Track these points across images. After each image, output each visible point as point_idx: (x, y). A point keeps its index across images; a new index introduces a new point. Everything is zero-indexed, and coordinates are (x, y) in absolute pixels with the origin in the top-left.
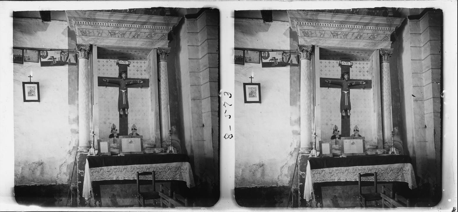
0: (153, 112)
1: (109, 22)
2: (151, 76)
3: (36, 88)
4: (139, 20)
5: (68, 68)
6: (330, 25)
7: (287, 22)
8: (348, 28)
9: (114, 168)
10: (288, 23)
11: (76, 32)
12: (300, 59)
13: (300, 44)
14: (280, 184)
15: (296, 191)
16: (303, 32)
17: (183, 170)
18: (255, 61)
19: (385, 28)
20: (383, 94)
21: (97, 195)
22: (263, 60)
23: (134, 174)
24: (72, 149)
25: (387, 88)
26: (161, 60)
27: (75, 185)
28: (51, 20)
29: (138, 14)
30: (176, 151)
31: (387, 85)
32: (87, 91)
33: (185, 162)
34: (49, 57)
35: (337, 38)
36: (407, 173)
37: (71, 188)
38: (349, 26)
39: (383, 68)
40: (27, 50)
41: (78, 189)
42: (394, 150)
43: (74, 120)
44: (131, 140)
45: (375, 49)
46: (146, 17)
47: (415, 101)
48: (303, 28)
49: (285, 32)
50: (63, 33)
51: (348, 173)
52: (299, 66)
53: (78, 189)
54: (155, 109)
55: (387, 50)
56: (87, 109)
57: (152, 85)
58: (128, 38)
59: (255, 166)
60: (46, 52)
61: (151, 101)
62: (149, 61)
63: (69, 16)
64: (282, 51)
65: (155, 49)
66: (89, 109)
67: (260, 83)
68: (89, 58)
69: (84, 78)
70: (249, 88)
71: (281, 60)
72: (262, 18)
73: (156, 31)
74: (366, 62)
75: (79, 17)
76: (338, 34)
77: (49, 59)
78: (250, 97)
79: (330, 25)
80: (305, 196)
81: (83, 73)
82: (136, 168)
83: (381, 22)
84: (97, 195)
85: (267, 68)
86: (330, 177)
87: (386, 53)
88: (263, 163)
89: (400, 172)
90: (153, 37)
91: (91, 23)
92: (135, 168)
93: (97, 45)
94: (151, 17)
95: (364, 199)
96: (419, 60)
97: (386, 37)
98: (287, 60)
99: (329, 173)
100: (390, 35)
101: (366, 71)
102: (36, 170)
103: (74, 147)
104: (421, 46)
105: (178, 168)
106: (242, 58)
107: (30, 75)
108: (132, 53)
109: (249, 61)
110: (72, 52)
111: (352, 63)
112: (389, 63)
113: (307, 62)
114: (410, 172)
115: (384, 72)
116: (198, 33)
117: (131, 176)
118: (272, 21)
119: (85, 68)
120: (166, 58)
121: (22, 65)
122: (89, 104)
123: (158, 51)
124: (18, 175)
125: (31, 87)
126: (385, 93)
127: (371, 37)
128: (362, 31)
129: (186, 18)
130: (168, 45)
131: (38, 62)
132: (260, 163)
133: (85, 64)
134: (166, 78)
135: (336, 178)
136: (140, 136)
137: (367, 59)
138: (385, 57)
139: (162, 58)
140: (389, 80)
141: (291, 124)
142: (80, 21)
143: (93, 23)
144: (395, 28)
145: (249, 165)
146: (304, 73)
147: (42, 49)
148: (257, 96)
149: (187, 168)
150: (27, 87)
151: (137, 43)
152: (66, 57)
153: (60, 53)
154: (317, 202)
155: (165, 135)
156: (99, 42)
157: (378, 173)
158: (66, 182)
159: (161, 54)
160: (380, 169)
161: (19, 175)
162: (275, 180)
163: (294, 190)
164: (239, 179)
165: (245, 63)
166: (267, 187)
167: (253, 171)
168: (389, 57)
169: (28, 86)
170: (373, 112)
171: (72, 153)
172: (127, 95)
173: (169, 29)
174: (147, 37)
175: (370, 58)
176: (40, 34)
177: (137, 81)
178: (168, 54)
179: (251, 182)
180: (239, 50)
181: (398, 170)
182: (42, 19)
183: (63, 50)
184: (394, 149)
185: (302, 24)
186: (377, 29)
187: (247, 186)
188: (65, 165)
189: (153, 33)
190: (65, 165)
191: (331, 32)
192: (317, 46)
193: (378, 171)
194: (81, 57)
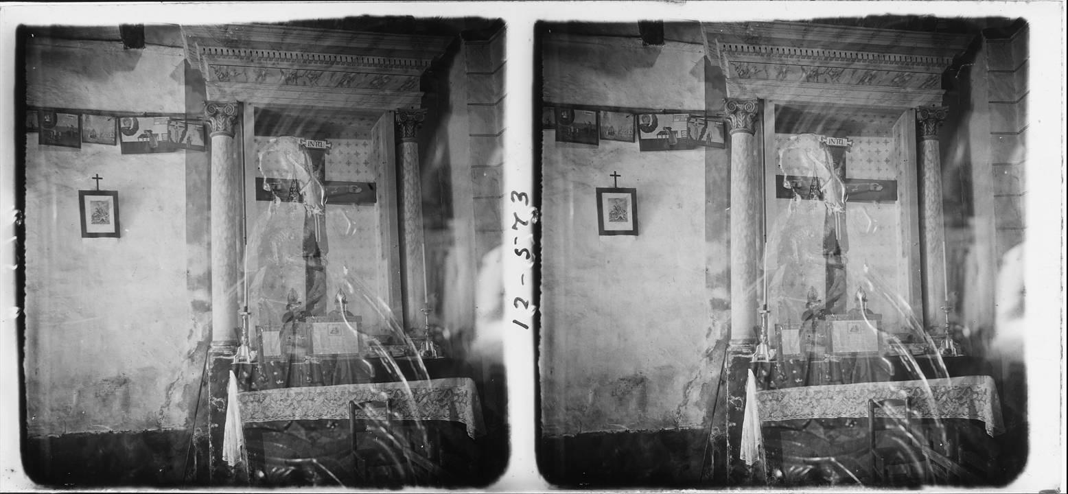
0: (907, 258)
1: (802, 47)
2: (901, 173)
3: (110, 206)
4: (874, 42)
5: (186, 158)
6: (801, 51)
7: (699, 44)
8: (843, 59)
9: (296, 393)
10: (702, 46)
11: (205, 74)
12: (210, 135)
13: (728, 96)
14: (165, 427)
15: (721, 442)
16: (216, 71)
17: (459, 397)
18: (105, 138)
19: (929, 58)
20: (925, 214)
21: (255, 454)
22: (641, 135)
23: (289, 406)
24: (196, 347)
25: (412, 202)
26: (925, 137)
27: (721, 430)
28: (145, 45)
29: (873, 27)
30: (440, 352)
31: (414, 196)
32: (231, 211)
33: (463, 379)
34: (659, 129)
35: (817, 82)
36: (981, 400)
37: (194, 440)
38: (846, 54)
39: (403, 156)
40: (608, 112)
41: (728, 441)
42: (949, 344)
43: (718, 279)
44: (334, 327)
45: (385, 110)
46: (892, 34)
47: (479, 233)
48: (216, 60)
49: (174, 72)
50: (173, 76)
51: (324, 401)
52: (728, 147)
53: (728, 441)
54: (910, 251)
55: (412, 114)
56: (749, 252)
57: (904, 195)
58: (327, 86)
59: (624, 382)
60: (134, 120)
61: (380, 236)
62: (897, 138)
63: (709, 32)
64: (687, 113)
65: (390, 111)
66: (755, 250)
67: (635, 189)
68: (235, 134)
69: (744, 179)
70: (92, 202)
71: (685, 133)
72: (639, 34)
73: (913, 68)
74: (884, 139)
75: (732, 33)
76: (298, 75)
77: (140, 137)
78: (94, 223)
79: (801, 51)
80: (227, 454)
81: (743, 166)
82: (868, 390)
83: (919, 45)
84: (255, 454)
85: (133, 155)
86: (801, 408)
87: (932, 117)
88: (643, 375)
89: (446, 399)
90: (908, 81)
91: (239, 51)
92: (346, 392)
93: (774, 100)
94: (903, 34)
95: (882, 459)
96: (487, 135)
97: (932, 79)
98: (700, 134)
99: (800, 399)
100: (419, 78)
101: (363, 161)
102: (111, 398)
103: (199, 343)
104: (491, 103)
105: (447, 392)
106: (593, 128)
107: (97, 175)
108: (334, 122)
109: (609, 137)
110: (714, 117)
111: (852, 141)
112: (937, 139)
113: (227, 141)
114: (988, 397)
115: (926, 162)
116: (492, 73)
117: (855, 409)
118: (663, 41)
119: (225, 158)
120: (937, 131)
121: (595, 148)
122: (235, 242)
123: (398, 118)
124: (585, 409)
125: (100, 203)
126: (929, 211)
127: (375, 82)
128: (305, 66)
129: (463, 40)
130: (941, 100)
131: (115, 144)
132: (637, 375)
133: (227, 148)
134: (415, 181)
135: (297, 412)
136: (876, 314)
137: (365, 135)
138: (928, 127)
139: (928, 131)
140: (417, 183)
141: (710, 286)
142: (735, 43)
143: (245, 52)
144: (430, 60)
145: (610, 380)
146: (740, 166)
147: (124, 114)
148: (110, 221)
149: (986, 389)
150: (89, 202)
151: (869, 96)
152: (180, 133)
153: (167, 122)
154: (770, 466)
155: (413, 314)
156: (260, 95)
157: (394, 400)
158: (700, 424)
159: (405, 124)
160: (918, 390)
161: (72, 410)
162: (670, 416)
163: (199, 439)
164: (587, 412)
165: (83, 144)
166: (651, 431)
167: (619, 393)
168: (937, 127)
169: (93, 200)
170: (901, 255)
171: (195, 356)
172: (844, 218)
173: (424, 64)
174: (371, 83)
175: (893, 129)
176: (119, 78)
177: (869, 186)
178: (941, 122)
179: (615, 421)
180: (68, 115)
181: (441, 394)
182: (125, 43)
183: (694, 111)
184: (951, 343)
185: (733, 48)
186: (388, 63)
187: (606, 431)
188: (697, 384)
189: (907, 73)
190: (180, 385)
191: (281, 71)
192: (771, 101)
193: (914, 395)
194: (217, 132)
